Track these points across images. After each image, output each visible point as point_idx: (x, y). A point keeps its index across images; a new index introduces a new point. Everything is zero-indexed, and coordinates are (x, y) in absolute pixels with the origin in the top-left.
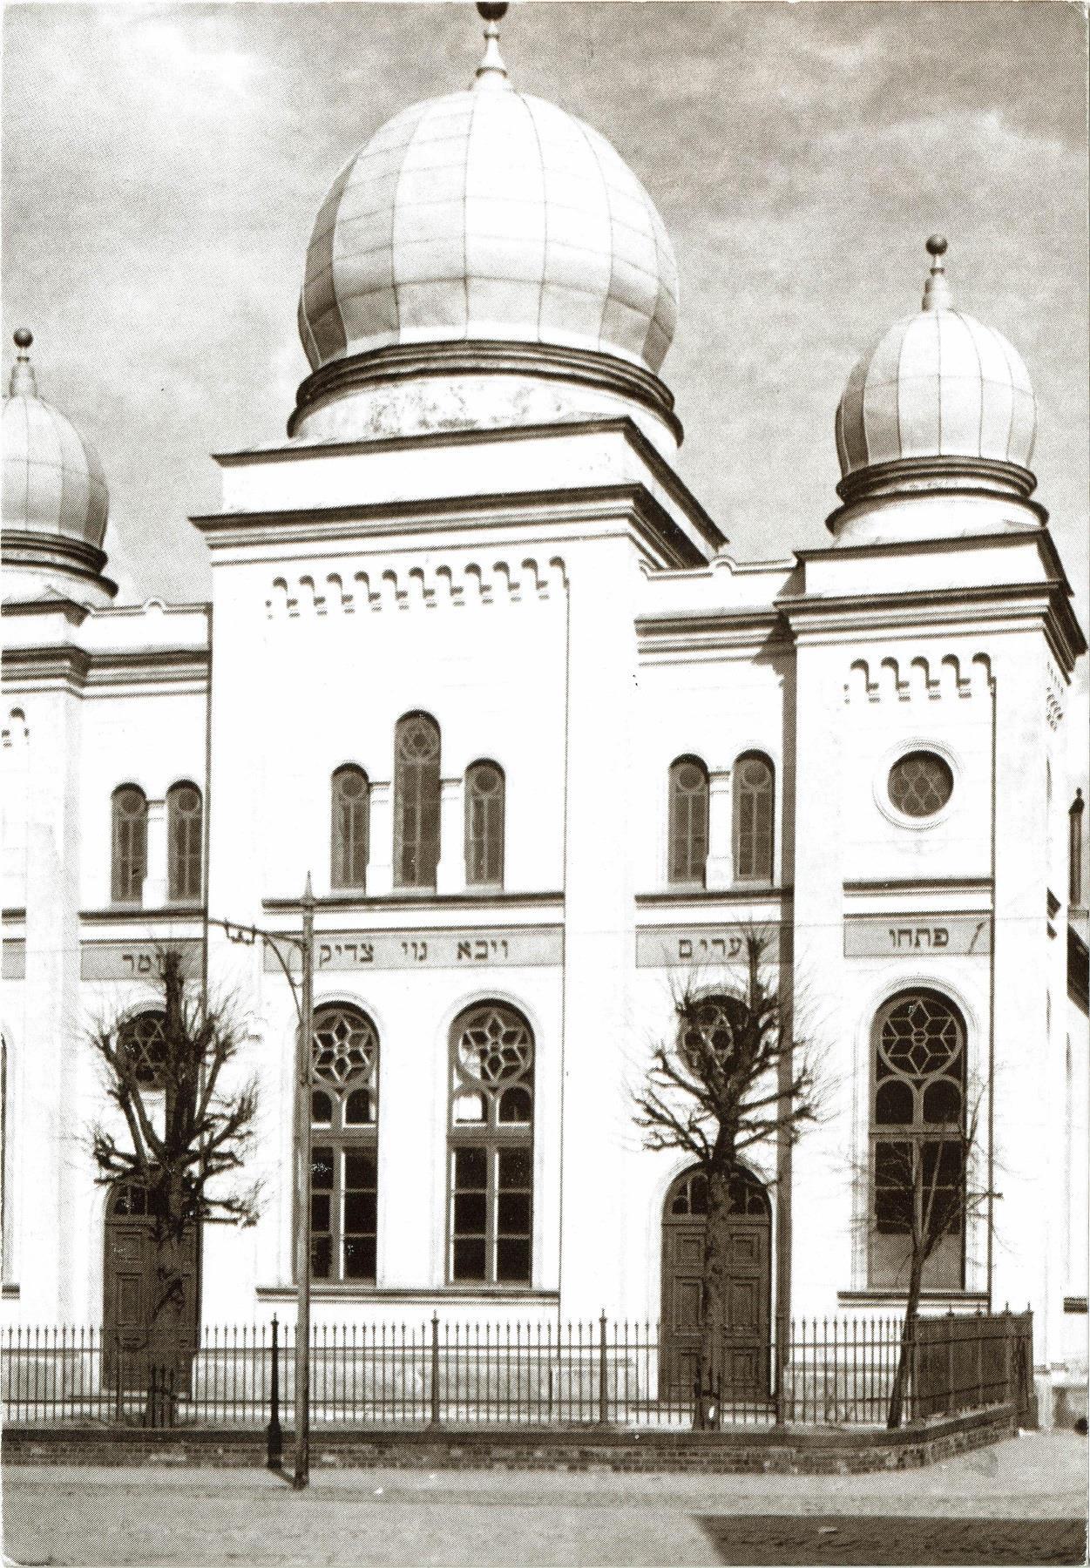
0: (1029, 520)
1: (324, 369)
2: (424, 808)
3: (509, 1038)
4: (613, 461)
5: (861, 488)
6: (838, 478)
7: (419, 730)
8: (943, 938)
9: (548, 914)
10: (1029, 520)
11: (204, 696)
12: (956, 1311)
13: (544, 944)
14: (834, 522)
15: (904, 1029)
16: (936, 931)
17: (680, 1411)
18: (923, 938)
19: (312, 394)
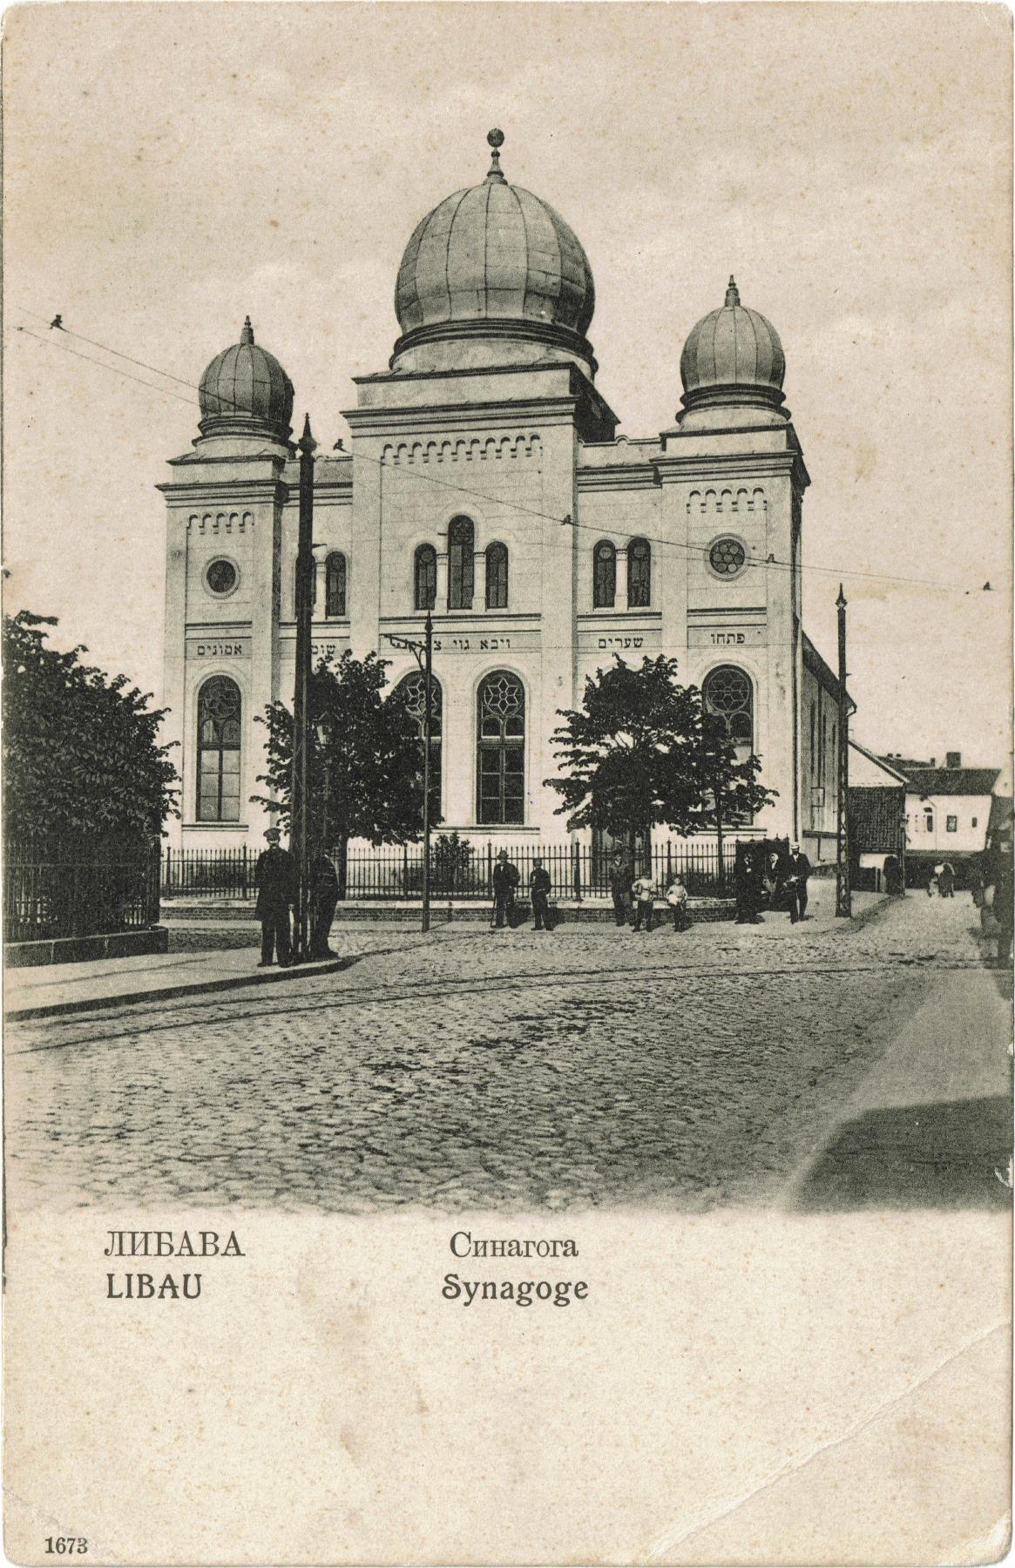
0: (779, 419)
1: (412, 333)
2: (462, 567)
3: (511, 690)
4: (553, 384)
5: (692, 401)
6: (682, 392)
7: (461, 529)
9: (534, 625)
10: (779, 419)
11: (779, 488)
12: (742, 839)
13: (527, 639)
14: (680, 417)
15: (737, 686)
17: (992, 833)
19: (401, 346)
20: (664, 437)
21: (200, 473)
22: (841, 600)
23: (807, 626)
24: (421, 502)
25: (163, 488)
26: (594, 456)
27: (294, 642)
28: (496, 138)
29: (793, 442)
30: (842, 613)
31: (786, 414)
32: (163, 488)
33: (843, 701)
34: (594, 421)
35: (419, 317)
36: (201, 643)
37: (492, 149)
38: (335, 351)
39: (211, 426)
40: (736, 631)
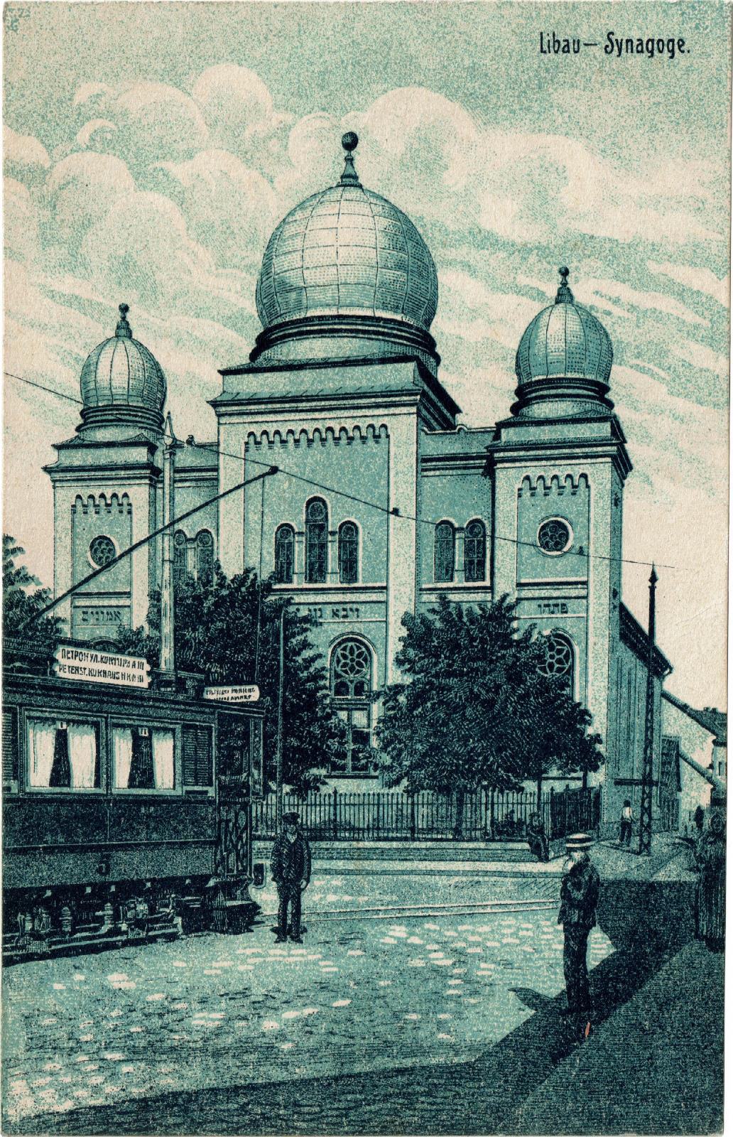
7: (316, 507)
10: (603, 409)
11: (601, 473)
20: (501, 425)
21: (78, 458)
22: (653, 579)
23: (626, 599)
24: (714, 71)
25: (47, 469)
27: (456, 568)
28: (351, 142)
29: (617, 431)
30: (652, 589)
31: (610, 405)
32: (47, 469)
33: (658, 665)
34: (437, 408)
36: (85, 610)
37: (345, 153)
38: (198, 353)
39: (91, 416)
40: (560, 601)
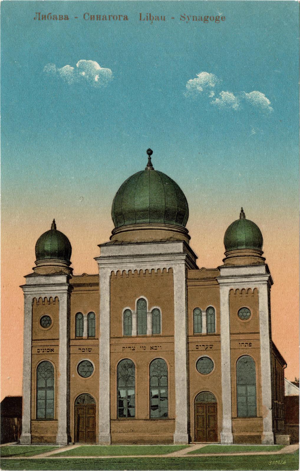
8: (251, 345)
16: (250, 343)
18: (247, 345)
19: (113, 233)
26: (193, 273)
35: (122, 215)
